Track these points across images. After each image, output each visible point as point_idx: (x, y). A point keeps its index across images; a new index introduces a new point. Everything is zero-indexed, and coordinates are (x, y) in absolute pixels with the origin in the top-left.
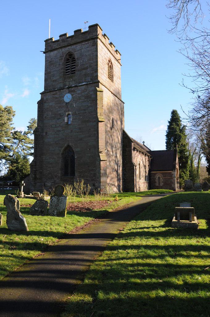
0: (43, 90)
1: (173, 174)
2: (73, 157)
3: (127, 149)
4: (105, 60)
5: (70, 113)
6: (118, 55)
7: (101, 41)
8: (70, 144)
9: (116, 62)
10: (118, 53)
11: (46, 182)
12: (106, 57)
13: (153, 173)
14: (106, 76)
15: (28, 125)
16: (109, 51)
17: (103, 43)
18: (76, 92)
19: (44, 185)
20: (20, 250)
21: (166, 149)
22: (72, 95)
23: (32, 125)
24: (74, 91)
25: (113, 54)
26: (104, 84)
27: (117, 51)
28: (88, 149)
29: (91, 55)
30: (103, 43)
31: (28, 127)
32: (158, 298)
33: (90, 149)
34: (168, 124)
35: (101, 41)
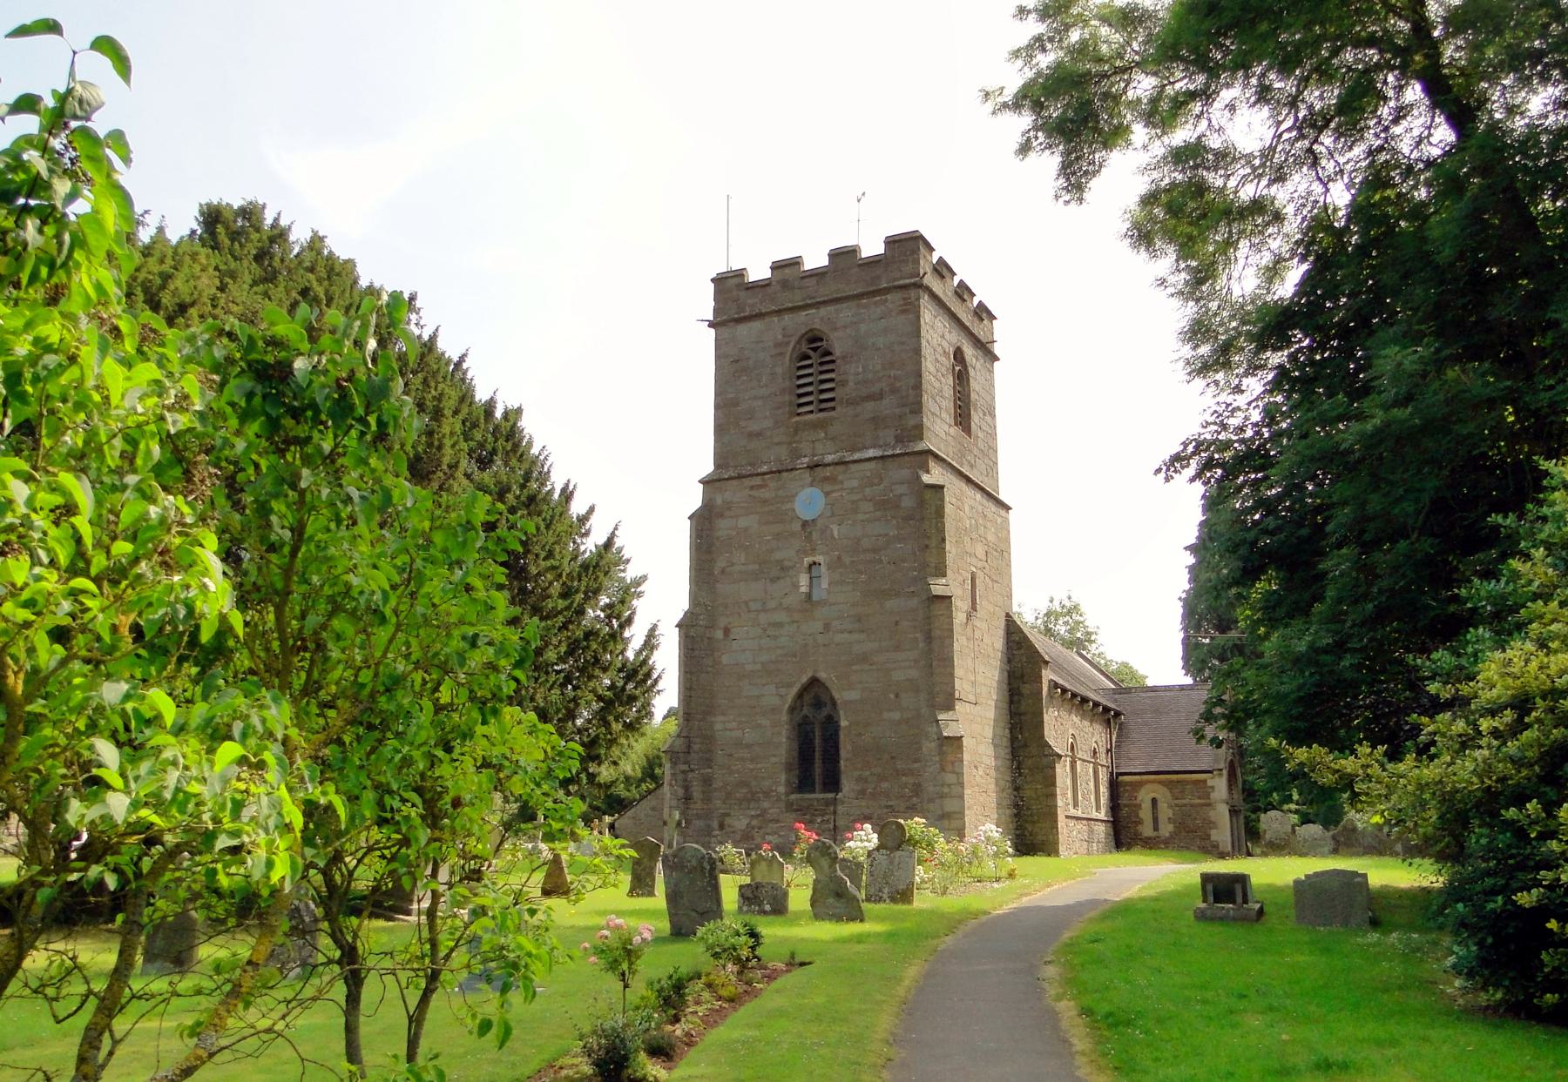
3: (1026, 689)
5: (819, 558)
8: (822, 675)
12: (945, 344)
24: (831, 480)
33: (897, 696)
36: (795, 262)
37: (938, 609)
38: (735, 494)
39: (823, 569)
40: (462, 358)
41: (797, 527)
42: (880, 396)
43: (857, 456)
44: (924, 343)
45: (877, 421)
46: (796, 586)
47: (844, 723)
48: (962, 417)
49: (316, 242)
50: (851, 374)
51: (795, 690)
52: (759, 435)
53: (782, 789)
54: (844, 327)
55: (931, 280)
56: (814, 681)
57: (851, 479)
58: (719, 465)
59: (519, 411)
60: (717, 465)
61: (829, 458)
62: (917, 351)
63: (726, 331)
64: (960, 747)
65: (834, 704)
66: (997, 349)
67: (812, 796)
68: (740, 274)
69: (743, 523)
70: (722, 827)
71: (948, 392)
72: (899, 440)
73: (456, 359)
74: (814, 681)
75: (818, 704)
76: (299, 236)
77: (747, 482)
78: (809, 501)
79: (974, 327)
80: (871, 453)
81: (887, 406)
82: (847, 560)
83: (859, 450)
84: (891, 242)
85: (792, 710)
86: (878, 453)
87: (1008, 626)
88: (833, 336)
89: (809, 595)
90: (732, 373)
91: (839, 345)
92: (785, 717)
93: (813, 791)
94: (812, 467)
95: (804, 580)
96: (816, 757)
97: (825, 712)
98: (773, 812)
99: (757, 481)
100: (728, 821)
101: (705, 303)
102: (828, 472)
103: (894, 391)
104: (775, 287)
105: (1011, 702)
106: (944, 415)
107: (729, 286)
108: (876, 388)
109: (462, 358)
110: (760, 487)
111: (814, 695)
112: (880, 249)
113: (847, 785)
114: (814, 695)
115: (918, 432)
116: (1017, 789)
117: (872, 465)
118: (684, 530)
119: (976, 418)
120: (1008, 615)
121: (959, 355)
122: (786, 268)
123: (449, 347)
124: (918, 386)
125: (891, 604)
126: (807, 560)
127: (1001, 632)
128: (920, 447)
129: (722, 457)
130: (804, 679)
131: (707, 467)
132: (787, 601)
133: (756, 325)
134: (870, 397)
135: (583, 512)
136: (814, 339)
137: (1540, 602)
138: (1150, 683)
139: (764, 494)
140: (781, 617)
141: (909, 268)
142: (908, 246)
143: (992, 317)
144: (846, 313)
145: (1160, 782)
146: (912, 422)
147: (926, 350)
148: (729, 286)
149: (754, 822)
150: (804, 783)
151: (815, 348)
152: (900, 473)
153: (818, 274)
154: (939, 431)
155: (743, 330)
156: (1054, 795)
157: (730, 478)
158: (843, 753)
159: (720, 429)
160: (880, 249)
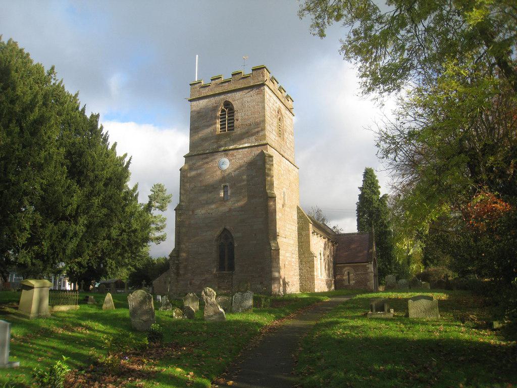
0: (188, 152)
1: (368, 268)
2: (232, 244)
3: (304, 233)
4: (273, 112)
5: (227, 184)
6: (290, 101)
7: (269, 87)
8: (228, 227)
9: (288, 112)
10: (289, 99)
11: (193, 279)
12: (275, 108)
13: (340, 267)
14: (275, 134)
15: (150, 194)
16: (279, 98)
17: (271, 89)
18: (236, 156)
19: (191, 284)
20: (152, 381)
21: (356, 231)
22: (230, 160)
23: (156, 194)
24: (233, 155)
25: (284, 102)
26: (273, 145)
27: (288, 96)
28: (253, 235)
29: (256, 107)
30: (271, 89)
31: (149, 197)
32: (359, 298)
33: (255, 235)
34: (360, 193)
35: (269, 87)
39: (229, 188)
40: (77, 95)
43: (241, 146)
44: (266, 106)
54: (236, 99)
56: (225, 229)
59: (98, 116)
62: (264, 108)
65: (232, 238)
67: (225, 272)
70: (191, 284)
71: (275, 124)
73: (73, 95)
74: (225, 229)
77: (201, 156)
80: (246, 145)
85: (217, 240)
86: (249, 145)
91: (236, 105)
93: (224, 271)
99: (204, 156)
100: (193, 281)
102: (231, 152)
106: (274, 132)
109: (77, 95)
110: (205, 158)
113: (237, 268)
114: (226, 235)
117: (247, 149)
121: (279, 111)
128: (265, 142)
131: (187, 151)
135: (122, 156)
136: (228, 104)
137: (175, 271)
138: (342, 232)
145: (350, 266)
147: (267, 108)
149: (203, 282)
150: (221, 267)
156: (314, 271)
157: (195, 155)
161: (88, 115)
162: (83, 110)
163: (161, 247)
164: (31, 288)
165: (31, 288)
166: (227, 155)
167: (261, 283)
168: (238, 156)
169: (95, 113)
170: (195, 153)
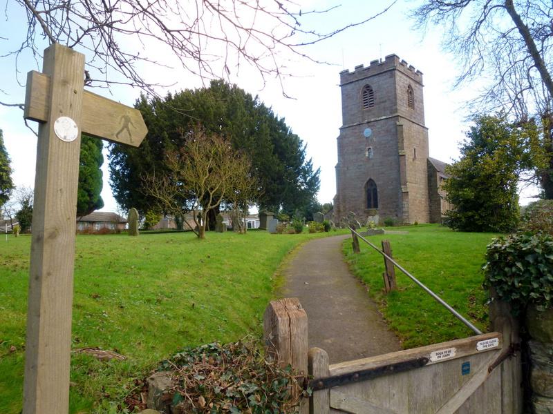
3: (433, 179)
5: (371, 147)
8: (372, 178)
24: (373, 125)
36: (361, 66)
37: (401, 158)
38: (349, 132)
41: (365, 139)
42: (385, 101)
45: (385, 109)
46: (365, 155)
47: (378, 190)
48: (411, 103)
49: (235, 86)
50: (377, 95)
51: (365, 182)
52: (354, 115)
53: (363, 208)
54: (375, 83)
55: (399, 67)
56: (370, 179)
57: (378, 125)
58: (344, 123)
59: (284, 119)
60: (344, 124)
61: (372, 120)
63: (344, 88)
64: (408, 195)
65: (376, 185)
66: (424, 84)
68: (347, 71)
69: (351, 139)
72: (391, 113)
74: (370, 179)
75: (372, 185)
76: (231, 86)
78: (368, 132)
79: (415, 77)
80: (384, 117)
81: (387, 104)
82: (378, 147)
83: (395, 113)
84: (387, 58)
85: (365, 187)
87: (428, 164)
88: (372, 86)
89: (368, 157)
90: (346, 98)
91: (374, 88)
92: (363, 189)
94: (368, 123)
95: (367, 153)
96: (372, 199)
97: (374, 187)
98: (361, 214)
101: (338, 81)
102: (372, 123)
103: (389, 99)
104: (357, 74)
105: (429, 183)
107: (345, 75)
108: (384, 100)
111: (371, 183)
112: (369, 65)
113: (380, 206)
114: (371, 183)
115: (396, 110)
116: (430, 206)
118: (336, 142)
119: (416, 104)
120: (428, 161)
121: (410, 87)
122: (359, 68)
123: (267, 105)
124: (396, 98)
125: (390, 158)
126: (367, 148)
127: (426, 164)
128: (396, 114)
129: (345, 122)
130: (368, 179)
131: (341, 125)
132: (363, 159)
133: (353, 84)
134: (383, 102)
136: (367, 87)
139: (357, 131)
140: (362, 163)
141: (393, 64)
142: (392, 58)
143: (421, 73)
144: (376, 79)
146: (394, 108)
147: (398, 87)
148: (345, 75)
150: (369, 206)
151: (368, 89)
152: (391, 122)
153: (368, 69)
154: (403, 109)
155: (349, 87)
158: (378, 198)
159: (344, 114)
160: (384, 60)
161: (279, 120)
162: (277, 118)
163: (326, 194)
164: (386, 249)
165: (386, 249)
166: (369, 127)
167: (397, 216)
168: (378, 126)
169: (283, 117)
170: (347, 126)
